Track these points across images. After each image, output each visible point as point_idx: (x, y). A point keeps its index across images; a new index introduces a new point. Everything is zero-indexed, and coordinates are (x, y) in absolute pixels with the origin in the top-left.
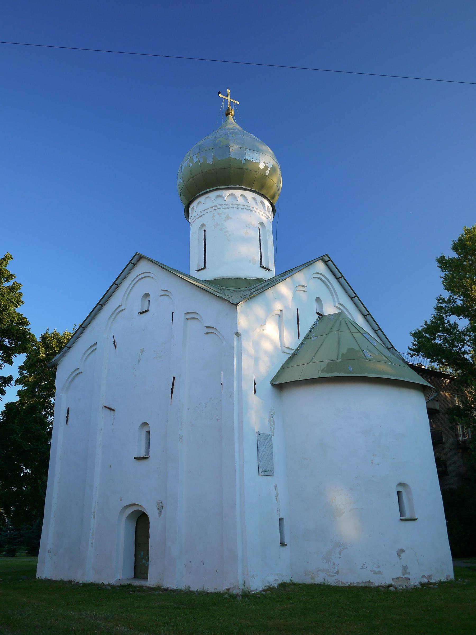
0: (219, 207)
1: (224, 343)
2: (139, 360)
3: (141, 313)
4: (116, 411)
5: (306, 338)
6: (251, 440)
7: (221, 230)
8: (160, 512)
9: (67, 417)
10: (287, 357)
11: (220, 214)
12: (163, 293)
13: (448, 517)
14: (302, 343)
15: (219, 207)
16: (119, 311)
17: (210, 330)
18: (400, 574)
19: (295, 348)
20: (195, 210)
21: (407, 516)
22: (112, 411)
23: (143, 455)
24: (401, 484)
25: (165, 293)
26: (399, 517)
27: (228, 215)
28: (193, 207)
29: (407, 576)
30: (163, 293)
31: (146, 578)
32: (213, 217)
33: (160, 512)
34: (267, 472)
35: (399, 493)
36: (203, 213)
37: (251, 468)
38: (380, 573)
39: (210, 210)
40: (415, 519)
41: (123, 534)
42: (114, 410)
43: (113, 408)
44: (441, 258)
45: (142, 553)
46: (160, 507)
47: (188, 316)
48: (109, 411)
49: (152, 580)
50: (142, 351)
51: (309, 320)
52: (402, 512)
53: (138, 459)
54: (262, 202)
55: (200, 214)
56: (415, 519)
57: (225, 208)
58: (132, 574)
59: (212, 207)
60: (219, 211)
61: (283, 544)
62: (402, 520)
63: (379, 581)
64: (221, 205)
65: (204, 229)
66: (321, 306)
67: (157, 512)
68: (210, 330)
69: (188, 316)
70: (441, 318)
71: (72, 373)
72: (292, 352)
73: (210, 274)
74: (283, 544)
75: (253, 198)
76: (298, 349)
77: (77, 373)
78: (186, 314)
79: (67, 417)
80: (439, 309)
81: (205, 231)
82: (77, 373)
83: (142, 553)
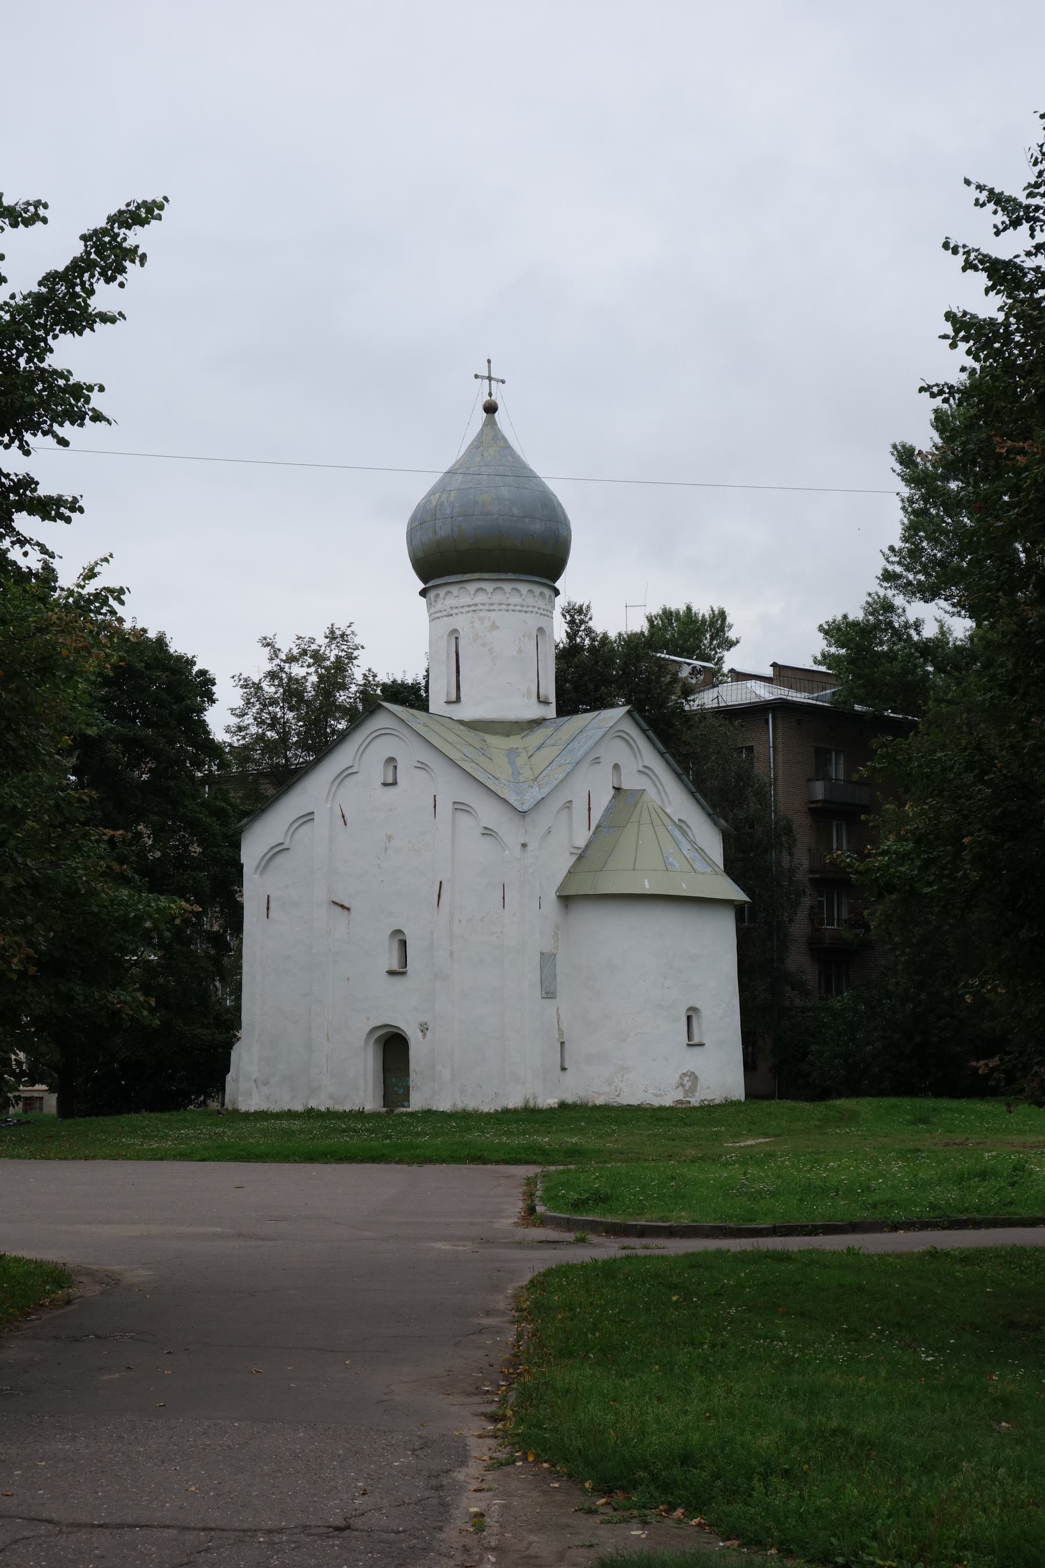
1: (507, 852)
2: (386, 849)
4: (352, 911)
5: (598, 827)
7: (484, 645)
8: (424, 1035)
10: (575, 858)
12: (419, 765)
13: (742, 1032)
14: (594, 833)
17: (488, 832)
18: (681, 1097)
21: (696, 1041)
22: (345, 912)
23: (395, 966)
25: (422, 767)
26: (686, 1041)
27: (494, 622)
28: (438, 595)
29: (688, 1099)
32: (472, 622)
33: (424, 1035)
35: (689, 1018)
38: (661, 1095)
40: (702, 1045)
42: (348, 909)
43: (347, 905)
45: (394, 1080)
46: (424, 1029)
47: (457, 806)
48: (339, 910)
49: (417, 1102)
50: (389, 838)
52: (690, 1036)
56: (702, 1045)
57: (489, 611)
58: (382, 1103)
59: (470, 606)
60: (482, 614)
61: (563, 1069)
62: (689, 1045)
63: (656, 1102)
64: (484, 604)
67: (421, 1034)
68: (488, 832)
69: (457, 806)
71: (272, 848)
72: (579, 852)
73: (467, 711)
74: (563, 1069)
75: (530, 591)
76: (587, 846)
77: (279, 850)
78: (454, 803)
79: (268, 908)
80: (888, 577)
81: (457, 638)
82: (279, 850)
83: (394, 1080)
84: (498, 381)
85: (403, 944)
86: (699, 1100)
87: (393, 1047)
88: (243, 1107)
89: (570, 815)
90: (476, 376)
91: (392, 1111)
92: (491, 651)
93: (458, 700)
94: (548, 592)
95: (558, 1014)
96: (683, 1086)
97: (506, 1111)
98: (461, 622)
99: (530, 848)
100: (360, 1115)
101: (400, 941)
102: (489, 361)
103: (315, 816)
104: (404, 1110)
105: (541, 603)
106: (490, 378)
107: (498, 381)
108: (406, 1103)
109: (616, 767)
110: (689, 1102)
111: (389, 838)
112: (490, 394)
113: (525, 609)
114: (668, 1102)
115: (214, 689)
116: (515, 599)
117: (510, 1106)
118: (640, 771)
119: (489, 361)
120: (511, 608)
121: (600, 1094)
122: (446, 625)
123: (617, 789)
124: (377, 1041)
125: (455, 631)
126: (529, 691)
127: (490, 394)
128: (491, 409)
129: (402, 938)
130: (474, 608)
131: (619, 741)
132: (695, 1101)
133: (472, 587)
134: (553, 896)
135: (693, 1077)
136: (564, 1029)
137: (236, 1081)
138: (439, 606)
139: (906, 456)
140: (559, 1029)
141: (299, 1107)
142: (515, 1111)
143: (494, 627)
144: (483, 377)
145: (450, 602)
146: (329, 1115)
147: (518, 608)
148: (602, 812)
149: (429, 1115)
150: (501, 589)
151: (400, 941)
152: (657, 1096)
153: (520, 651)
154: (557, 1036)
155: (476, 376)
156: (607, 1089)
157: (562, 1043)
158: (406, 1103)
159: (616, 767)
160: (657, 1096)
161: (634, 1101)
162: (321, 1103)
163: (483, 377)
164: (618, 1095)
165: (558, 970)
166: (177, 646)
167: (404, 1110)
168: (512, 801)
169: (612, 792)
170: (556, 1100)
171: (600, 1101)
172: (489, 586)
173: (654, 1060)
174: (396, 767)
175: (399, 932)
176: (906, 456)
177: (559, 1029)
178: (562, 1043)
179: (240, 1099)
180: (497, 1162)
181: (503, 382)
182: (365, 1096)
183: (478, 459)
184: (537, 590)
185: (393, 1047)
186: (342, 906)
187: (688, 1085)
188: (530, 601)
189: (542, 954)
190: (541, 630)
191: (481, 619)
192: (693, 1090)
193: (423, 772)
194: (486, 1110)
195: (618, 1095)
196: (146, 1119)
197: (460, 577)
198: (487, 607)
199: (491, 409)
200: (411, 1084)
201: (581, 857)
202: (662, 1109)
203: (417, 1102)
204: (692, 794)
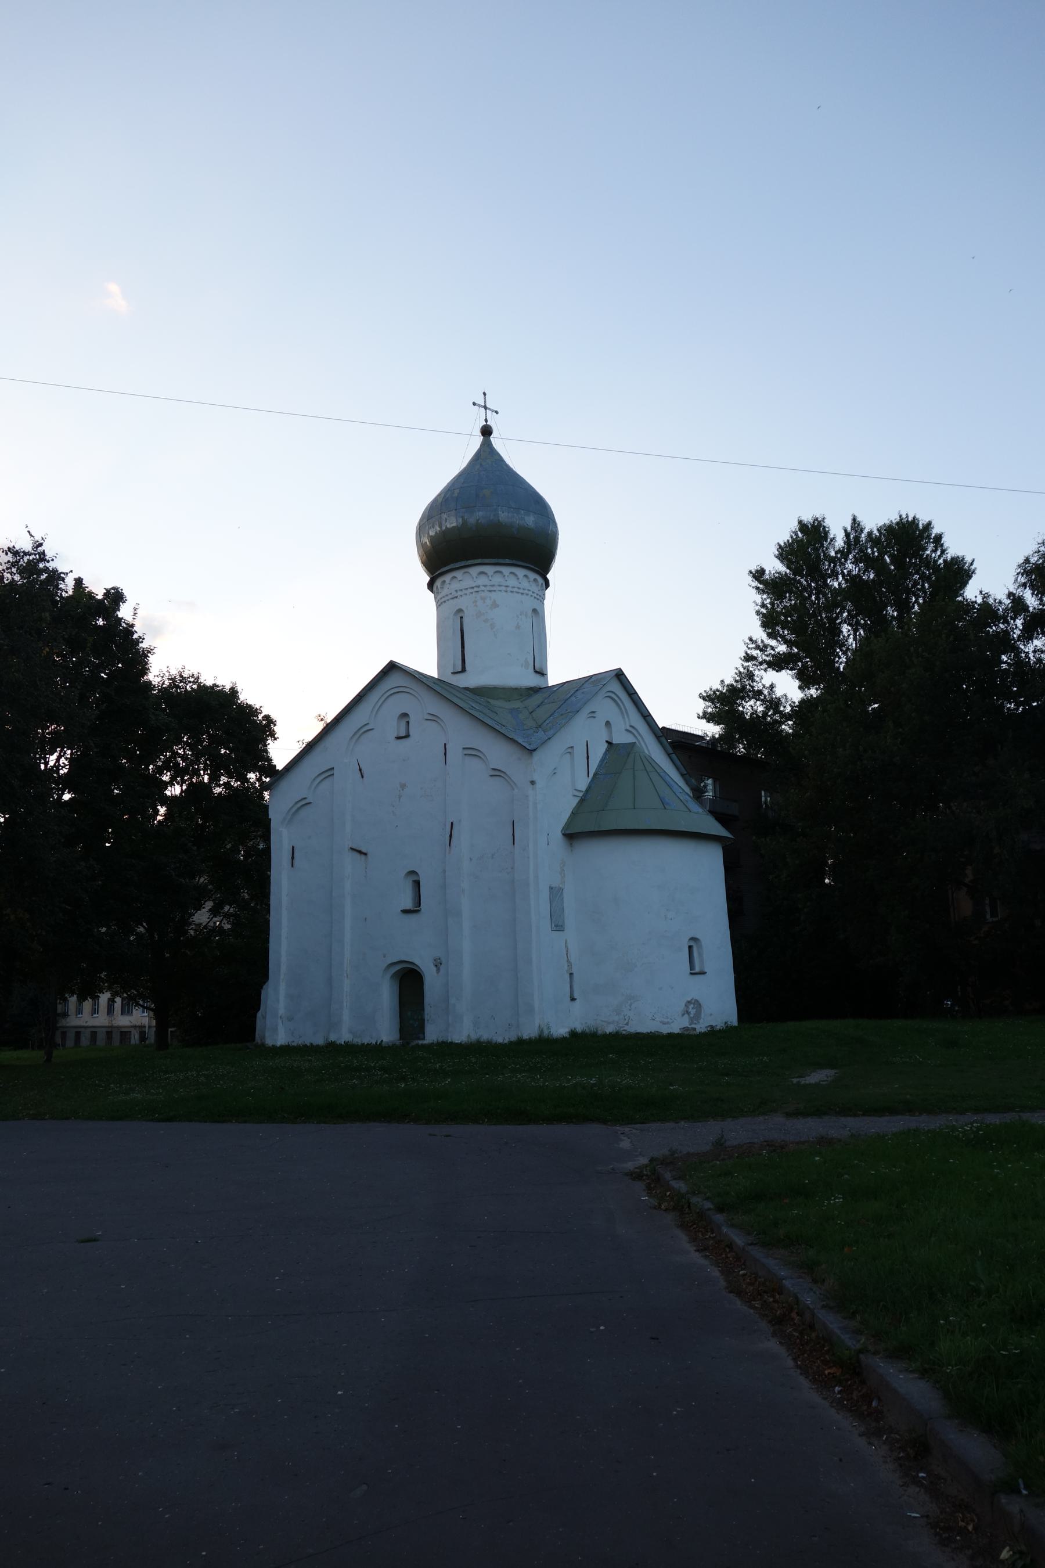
0: (482, 588)
2: (400, 797)
3: (398, 738)
4: (369, 856)
5: (595, 775)
6: (545, 895)
7: (486, 621)
8: (438, 970)
9: (293, 858)
10: (577, 800)
11: (483, 599)
12: (430, 717)
14: (592, 780)
15: (482, 588)
16: (364, 730)
17: (497, 773)
18: (687, 1025)
19: (584, 790)
20: (446, 586)
21: (697, 970)
22: (363, 856)
23: (409, 905)
24: (692, 939)
25: (434, 718)
26: (689, 971)
28: (444, 582)
30: (430, 717)
31: (424, 1039)
32: (475, 602)
33: (438, 970)
34: (558, 927)
35: (690, 947)
36: (460, 593)
37: (546, 924)
38: (668, 1023)
39: (470, 590)
40: (703, 973)
41: (386, 997)
42: (365, 854)
43: (364, 850)
44: (757, 571)
45: (409, 1013)
46: (438, 964)
48: (357, 855)
49: (432, 1034)
50: (403, 786)
51: (598, 751)
53: (406, 912)
54: (535, 580)
55: (455, 594)
60: (483, 594)
61: (573, 999)
63: (665, 1030)
64: (485, 586)
65: (461, 615)
66: (610, 732)
68: (497, 773)
70: (751, 676)
71: (297, 803)
72: (581, 794)
74: (573, 999)
75: (525, 576)
76: (587, 791)
77: (304, 804)
79: (293, 858)
80: (748, 658)
83: (409, 1013)
84: (492, 411)
85: (417, 884)
86: (703, 1026)
87: (409, 981)
88: (269, 1042)
89: (572, 759)
90: (474, 404)
91: (408, 1043)
92: (492, 626)
93: (463, 670)
94: (540, 580)
95: (566, 946)
96: (688, 1013)
97: (520, 1042)
98: (464, 602)
99: (538, 786)
100: (376, 1050)
101: (414, 881)
102: (485, 394)
103: (335, 772)
104: (420, 1042)
105: (534, 588)
106: (485, 408)
107: (492, 411)
108: (421, 1036)
109: (608, 723)
110: (695, 1029)
111: (403, 786)
112: (486, 421)
113: (521, 591)
114: (675, 1029)
115: (276, 729)
116: (512, 582)
117: (526, 1036)
118: (627, 730)
119: (485, 394)
120: (509, 589)
121: (609, 1023)
122: (452, 606)
123: (609, 743)
124: (395, 975)
125: (460, 610)
126: (526, 661)
127: (486, 421)
128: (486, 431)
129: (415, 878)
130: (476, 589)
131: (609, 700)
132: (701, 1027)
133: (474, 571)
134: (559, 835)
135: (697, 1004)
136: (572, 960)
137: (264, 1017)
138: (445, 591)
139: (758, 575)
140: (568, 961)
141: (319, 1041)
142: (530, 1042)
143: (495, 605)
144: (480, 406)
145: (455, 585)
146: (349, 1048)
147: (516, 590)
148: (598, 762)
149: (445, 1049)
150: (500, 572)
151: (414, 881)
152: (664, 1023)
153: (518, 627)
154: (566, 967)
155: (474, 404)
156: (616, 1018)
157: (571, 974)
158: (421, 1036)
159: (608, 723)
160: (664, 1023)
161: (644, 1029)
162: (343, 1036)
163: (480, 406)
164: (627, 1024)
165: (565, 905)
166: (246, 697)
167: (420, 1042)
168: (520, 741)
169: (606, 745)
170: (567, 1030)
171: (610, 1029)
172: (489, 570)
173: (660, 989)
174: (408, 722)
175: (413, 873)
176: (758, 575)
177: (568, 961)
178: (571, 974)
179: (267, 1034)
180: (549, 1120)
181: (497, 412)
182: (385, 1030)
183: (478, 467)
184: (532, 576)
185: (409, 981)
186: (360, 852)
187: (693, 1012)
188: (525, 584)
189: (551, 888)
190: (535, 611)
191: (483, 599)
192: (698, 1016)
193: (434, 724)
194: (500, 1040)
195: (627, 1024)
196: (398, 1027)
197: (463, 563)
198: (489, 588)
199: (486, 431)
200: (426, 1017)
201: (582, 801)
202: (670, 1035)
203: (432, 1034)
204: (669, 755)
